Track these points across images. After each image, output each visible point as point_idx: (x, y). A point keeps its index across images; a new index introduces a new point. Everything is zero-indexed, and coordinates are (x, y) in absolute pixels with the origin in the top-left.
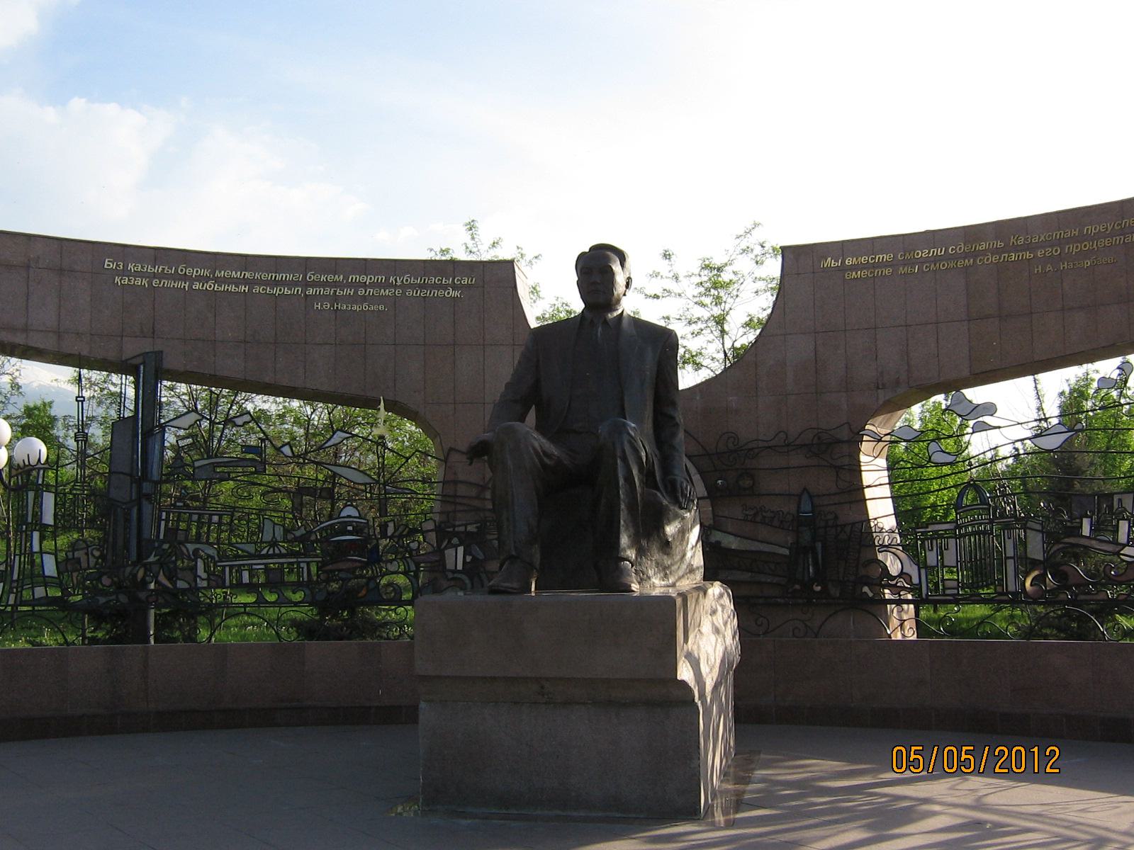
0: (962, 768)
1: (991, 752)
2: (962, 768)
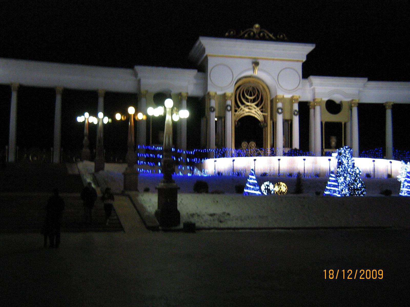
0: (379, 277)
1: (358, 271)
2: (379, 277)
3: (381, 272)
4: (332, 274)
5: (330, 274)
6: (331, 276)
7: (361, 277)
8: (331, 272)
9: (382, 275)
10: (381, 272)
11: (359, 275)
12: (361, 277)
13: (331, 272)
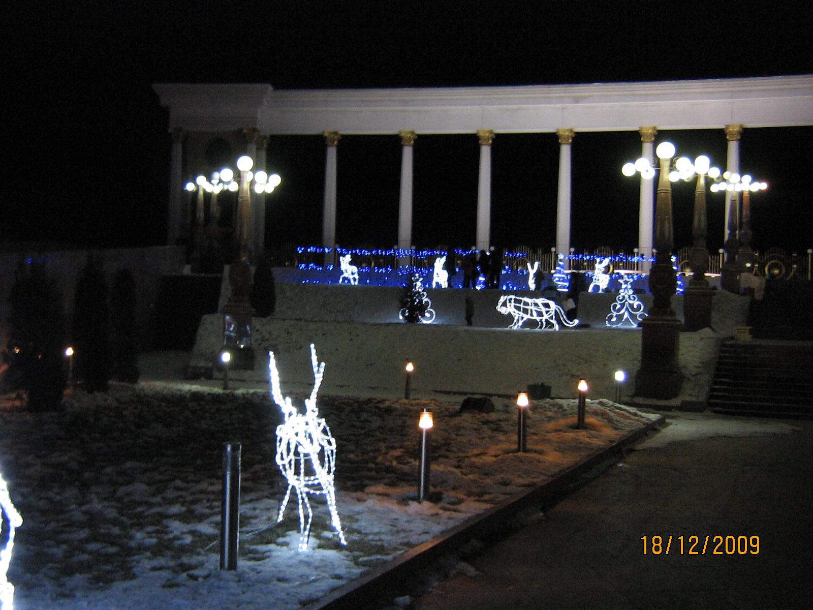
0: (751, 551)
2: (751, 551)
3: (755, 542)
4: (659, 545)
5: (655, 545)
6: (657, 549)
7: (692, 551)
8: (657, 541)
9: (758, 545)
10: (755, 542)
11: (711, 545)
12: (692, 551)
13: (657, 541)
